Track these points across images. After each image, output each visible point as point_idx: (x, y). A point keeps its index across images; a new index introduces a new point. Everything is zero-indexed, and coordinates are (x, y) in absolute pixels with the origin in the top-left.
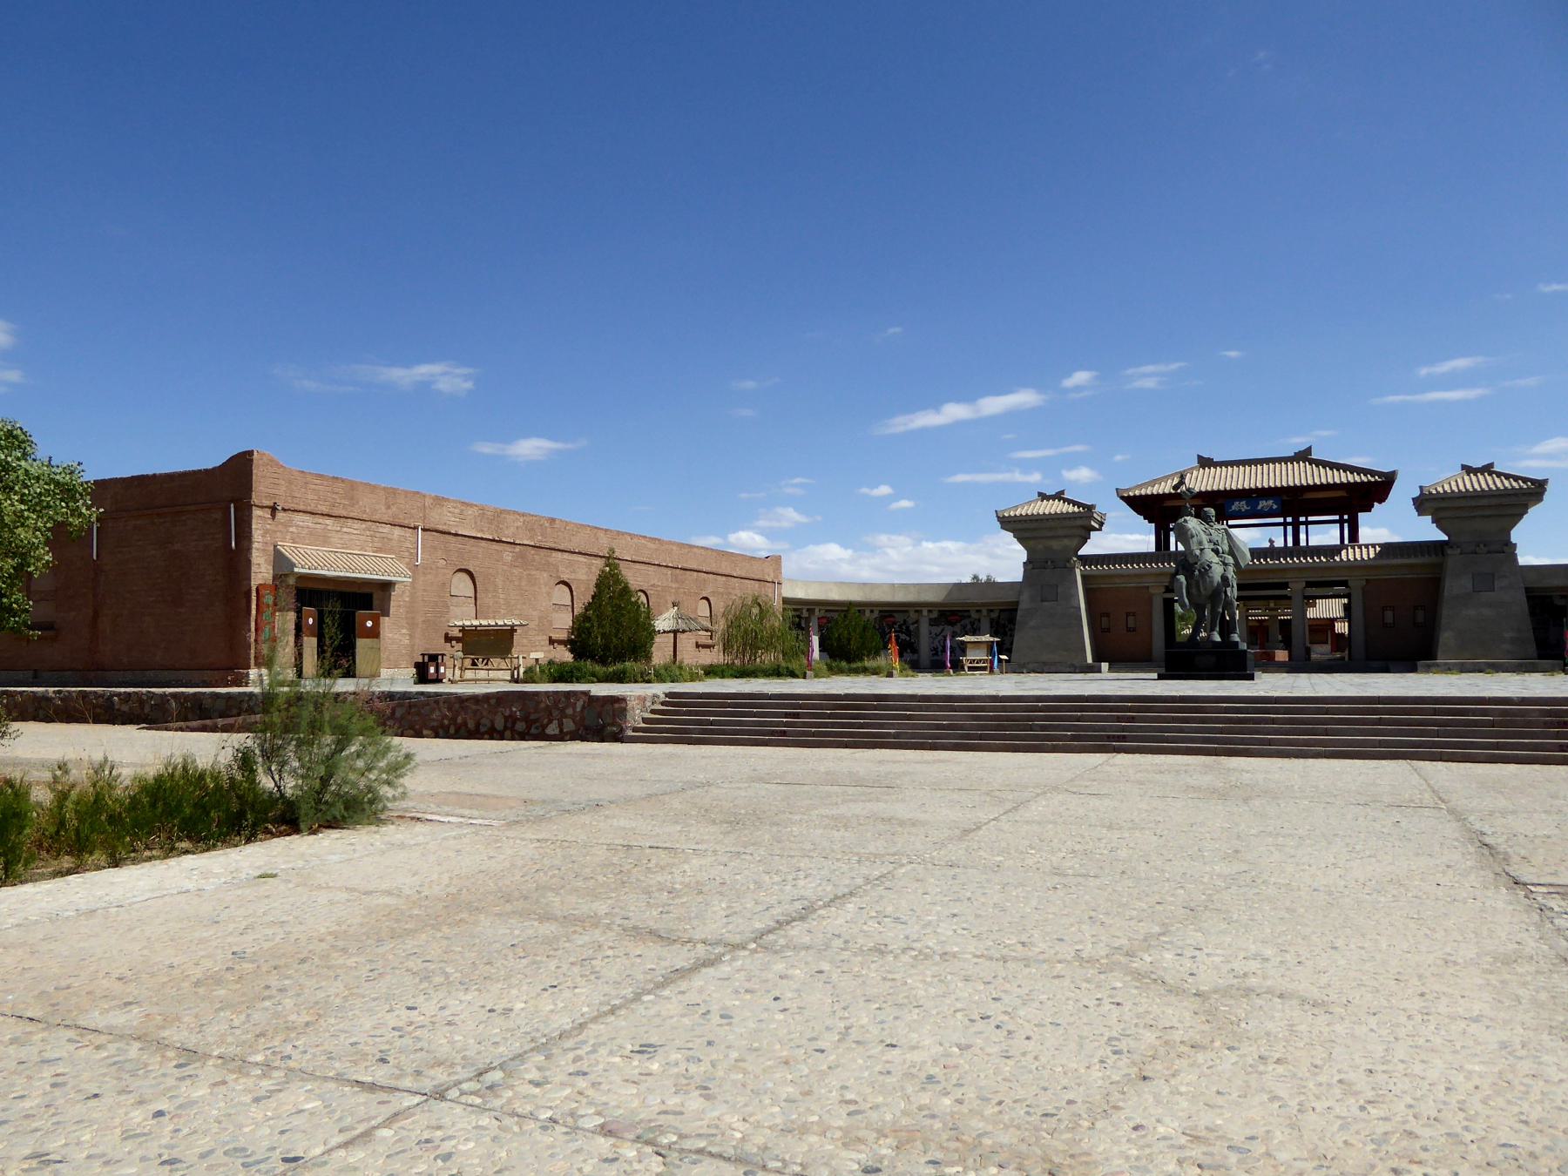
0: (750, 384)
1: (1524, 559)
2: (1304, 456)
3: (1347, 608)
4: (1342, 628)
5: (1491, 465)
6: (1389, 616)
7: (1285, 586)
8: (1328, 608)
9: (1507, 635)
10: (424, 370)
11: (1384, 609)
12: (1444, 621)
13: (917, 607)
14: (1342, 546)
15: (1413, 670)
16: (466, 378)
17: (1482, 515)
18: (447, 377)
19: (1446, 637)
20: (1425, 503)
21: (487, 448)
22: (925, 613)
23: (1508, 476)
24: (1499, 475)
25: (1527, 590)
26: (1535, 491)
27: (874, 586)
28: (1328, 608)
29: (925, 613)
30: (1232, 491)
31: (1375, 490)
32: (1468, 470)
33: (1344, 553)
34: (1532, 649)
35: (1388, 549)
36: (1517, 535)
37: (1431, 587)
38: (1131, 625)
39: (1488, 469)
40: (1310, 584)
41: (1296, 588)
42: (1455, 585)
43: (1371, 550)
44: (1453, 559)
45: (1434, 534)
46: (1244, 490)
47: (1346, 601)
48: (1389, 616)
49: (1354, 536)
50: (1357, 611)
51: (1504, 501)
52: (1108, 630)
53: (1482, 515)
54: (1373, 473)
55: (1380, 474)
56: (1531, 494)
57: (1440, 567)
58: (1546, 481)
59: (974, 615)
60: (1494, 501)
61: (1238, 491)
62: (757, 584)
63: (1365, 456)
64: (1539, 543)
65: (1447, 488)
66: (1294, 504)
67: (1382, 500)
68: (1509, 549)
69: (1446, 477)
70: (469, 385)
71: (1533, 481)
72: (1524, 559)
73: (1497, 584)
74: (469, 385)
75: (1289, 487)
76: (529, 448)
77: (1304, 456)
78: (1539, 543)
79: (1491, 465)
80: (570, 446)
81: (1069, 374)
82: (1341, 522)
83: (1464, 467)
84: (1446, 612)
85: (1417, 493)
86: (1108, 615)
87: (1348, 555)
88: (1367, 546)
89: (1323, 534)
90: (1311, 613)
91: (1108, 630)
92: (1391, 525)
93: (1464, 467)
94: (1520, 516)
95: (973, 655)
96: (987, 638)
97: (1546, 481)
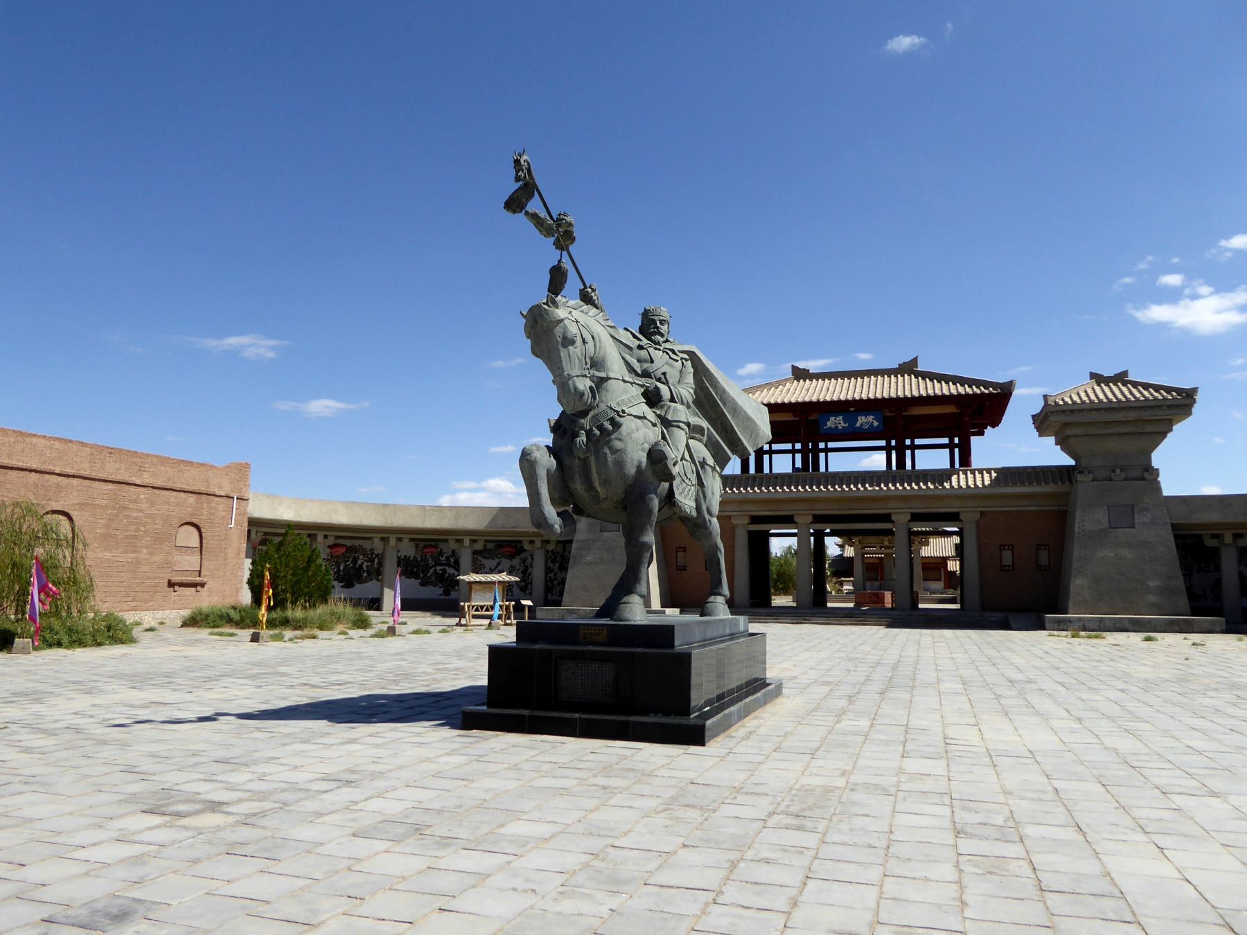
0: (500, 364)
1: (1166, 492)
2: (909, 368)
3: (959, 548)
4: (954, 566)
5: (1125, 373)
6: (1007, 557)
7: (886, 518)
8: (940, 547)
9: (1152, 584)
10: (233, 341)
11: (1001, 548)
12: (1075, 564)
13: (457, 535)
14: (952, 471)
15: (1040, 626)
16: (272, 348)
17: (1120, 428)
18: (253, 346)
19: (1078, 585)
20: (1050, 420)
21: (283, 406)
22: (467, 542)
23: (1146, 386)
24: (1135, 384)
25: (1174, 527)
26: (1180, 403)
27: (396, 508)
28: (940, 547)
29: (467, 542)
30: (825, 402)
31: (985, 407)
32: (1098, 379)
33: (954, 478)
34: (1183, 602)
35: (1007, 475)
36: (1159, 458)
37: (1057, 523)
38: (680, 562)
39: (1121, 378)
40: (916, 517)
41: (901, 518)
42: (1088, 519)
43: (986, 476)
44: (1084, 487)
45: (1059, 458)
46: (839, 401)
47: (956, 540)
48: (1007, 557)
49: (966, 460)
50: (971, 551)
51: (1145, 415)
52: (684, 568)
53: (1120, 428)
54: (986, 384)
55: (995, 385)
56: (1177, 406)
57: (1065, 497)
58: (1194, 390)
59: (527, 546)
60: (1132, 415)
61: (832, 402)
62: (192, 499)
63: (982, 365)
64: (1190, 467)
65: (1075, 398)
66: (897, 422)
67: (995, 424)
68: (1149, 475)
69: (1075, 388)
70: (272, 355)
71: (1179, 391)
72: (1166, 492)
73: (1138, 520)
74: (272, 355)
75: (891, 399)
76: (320, 406)
77: (909, 368)
78: (1190, 467)
79: (1125, 373)
80: (353, 407)
81: (743, 366)
82: (951, 446)
83: (1093, 376)
84: (1077, 552)
85: (1037, 407)
86: (684, 550)
87: (960, 481)
88: (981, 471)
89: (932, 458)
90: (926, 552)
91: (684, 568)
92: (1012, 445)
93: (1093, 376)
94: (1163, 435)
95: (479, 599)
96: (504, 577)
97: (1194, 390)
